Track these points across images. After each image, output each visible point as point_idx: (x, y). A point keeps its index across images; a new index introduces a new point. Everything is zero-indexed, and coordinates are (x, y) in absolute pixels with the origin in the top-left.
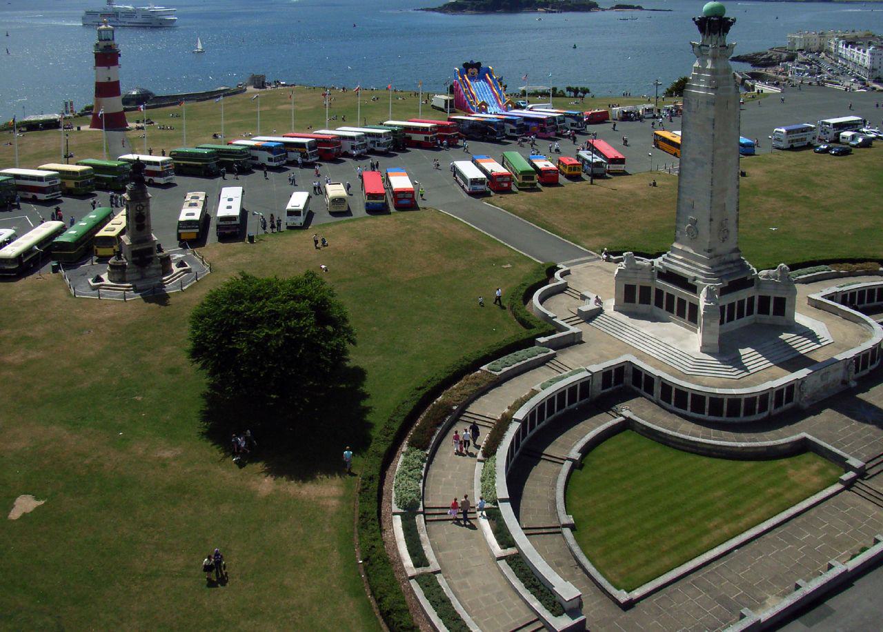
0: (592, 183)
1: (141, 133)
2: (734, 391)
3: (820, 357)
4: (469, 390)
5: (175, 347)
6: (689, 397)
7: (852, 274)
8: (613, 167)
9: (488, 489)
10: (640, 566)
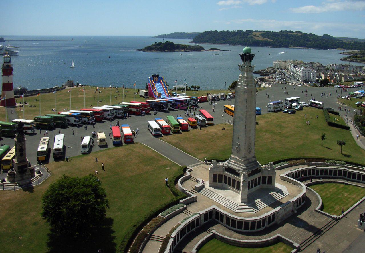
0: (201, 129)
2: (253, 218)
4: (153, 225)
7: (296, 165)
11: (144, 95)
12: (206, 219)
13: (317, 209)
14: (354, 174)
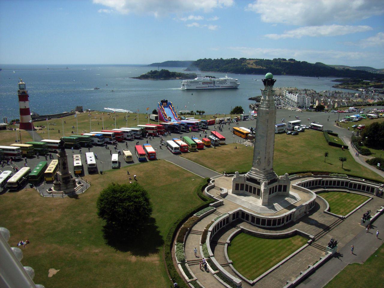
0: (215, 148)
1: (41, 131)
2: (275, 217)
3: (298, 205)
4: (192, 223)
5: (87, 214)
6: (261, 220)
7: (304, 177)
8: (221, 142)
9: (206, 254)
10: (254, 273)
11: (154, 119)
12: (234, 218)
13: (326, 211)
14: (355, 185)
